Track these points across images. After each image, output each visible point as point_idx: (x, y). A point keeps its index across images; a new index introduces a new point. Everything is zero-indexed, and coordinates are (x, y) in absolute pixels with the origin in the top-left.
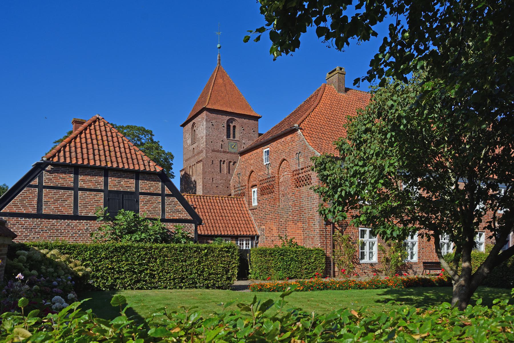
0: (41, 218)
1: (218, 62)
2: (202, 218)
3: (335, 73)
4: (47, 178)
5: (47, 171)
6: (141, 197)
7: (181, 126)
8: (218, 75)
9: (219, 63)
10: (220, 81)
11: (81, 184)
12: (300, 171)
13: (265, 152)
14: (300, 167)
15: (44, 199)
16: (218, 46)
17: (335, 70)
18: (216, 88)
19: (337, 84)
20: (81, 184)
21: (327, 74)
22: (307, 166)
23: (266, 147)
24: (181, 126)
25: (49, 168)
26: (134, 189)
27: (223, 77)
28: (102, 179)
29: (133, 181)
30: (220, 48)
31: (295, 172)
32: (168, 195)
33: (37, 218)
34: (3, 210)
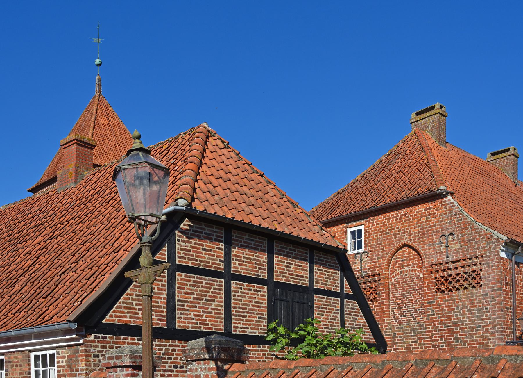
0: (174, 339)
1: (97, 88)
2: (298, 347)
3: (431, 112)
4: (186, 248)
5: (183, 232)
6: (317, 297)
7: (29, 191)
8: (99, 111)
9: (100, 91)
10: (104, 120)
11: (235, 265)
12: (451, 266)
13: (353, 233)
14: (451, 259)
15: (178, 296)
16: (98, 61)
17: (433, 108)
18: (98, 131)
19: (436, 131)
20: (236, 266)
21: (413, 115)
22: (469, 256)
23: (355, 224)
24: (29, 191)
25: (186, 224)
26: (306, 282)
27: (107, 115)
28: (265, 257)
29: (305, 265)
30: (100, 65)
31: (435, 267)
32: (348, 297)
33: (167, 339)
34: (107, 317)
